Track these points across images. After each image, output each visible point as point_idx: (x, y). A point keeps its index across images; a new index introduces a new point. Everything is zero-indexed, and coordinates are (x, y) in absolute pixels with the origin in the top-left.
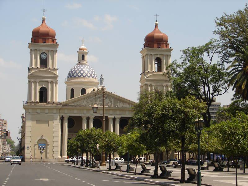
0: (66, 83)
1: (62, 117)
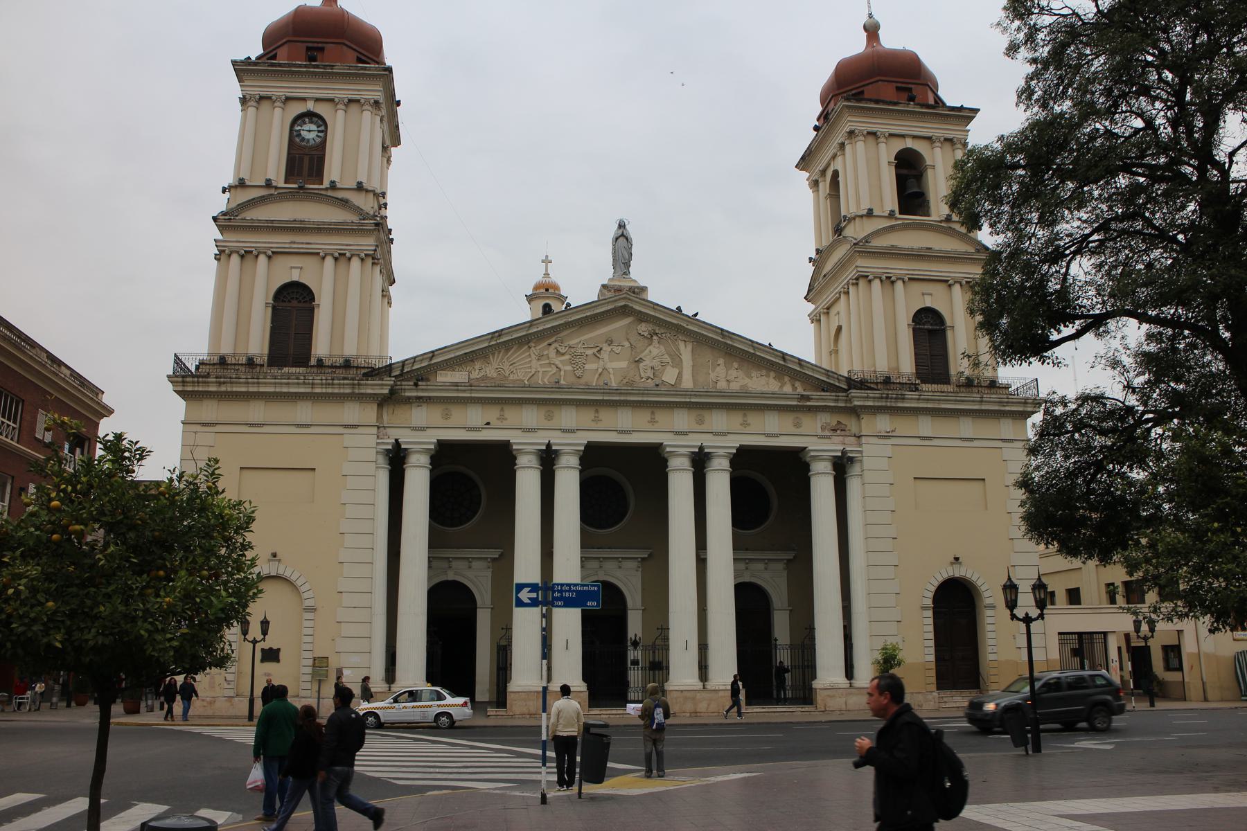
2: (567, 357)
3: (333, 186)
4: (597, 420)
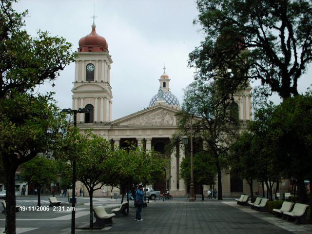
1: (112, 139)
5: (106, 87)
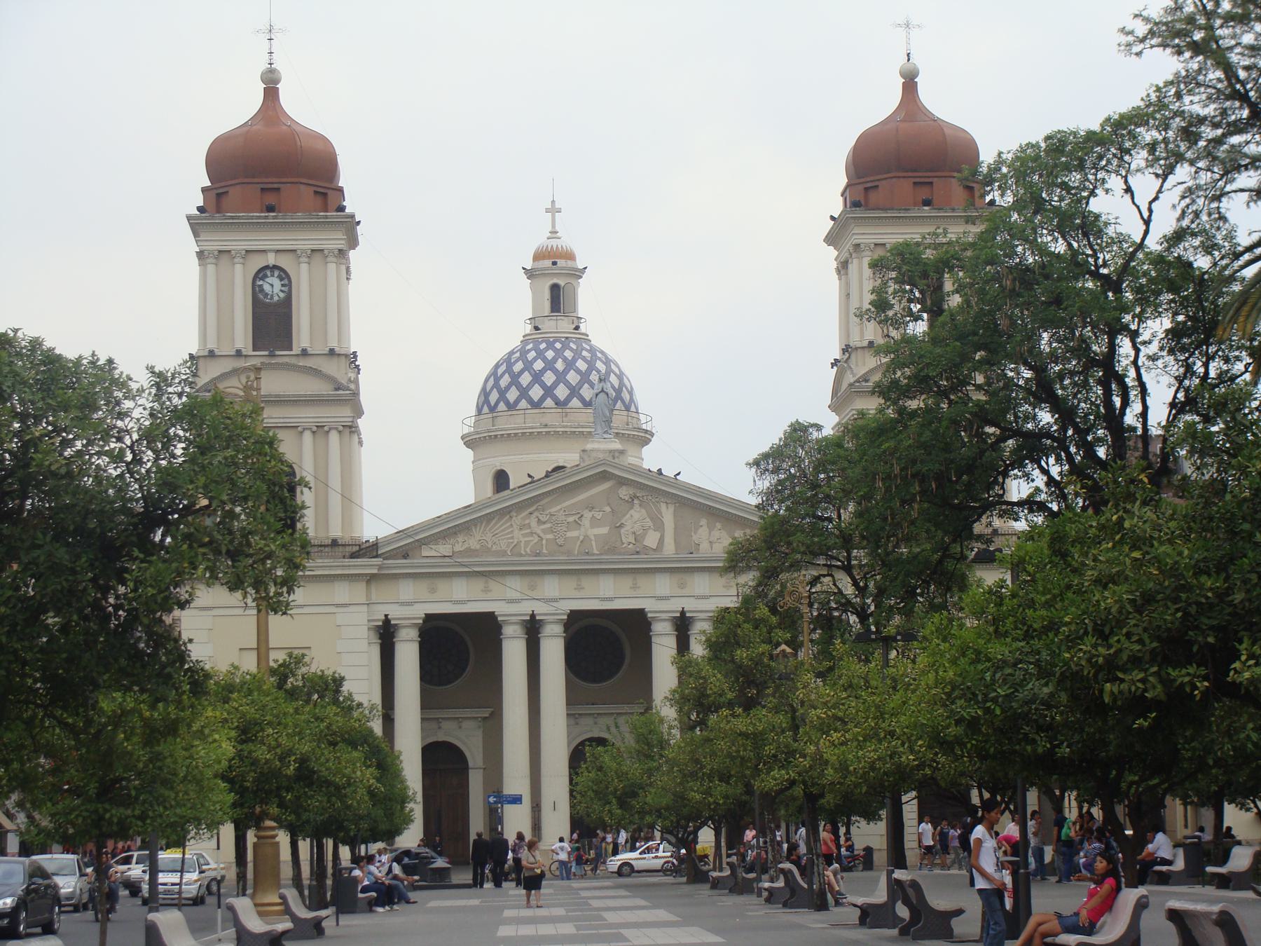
0: (470, 442)
1: (387, 621)
2: (548, 525)
3: (304, 353)
4: (486, 590)
5: (333, 368)
